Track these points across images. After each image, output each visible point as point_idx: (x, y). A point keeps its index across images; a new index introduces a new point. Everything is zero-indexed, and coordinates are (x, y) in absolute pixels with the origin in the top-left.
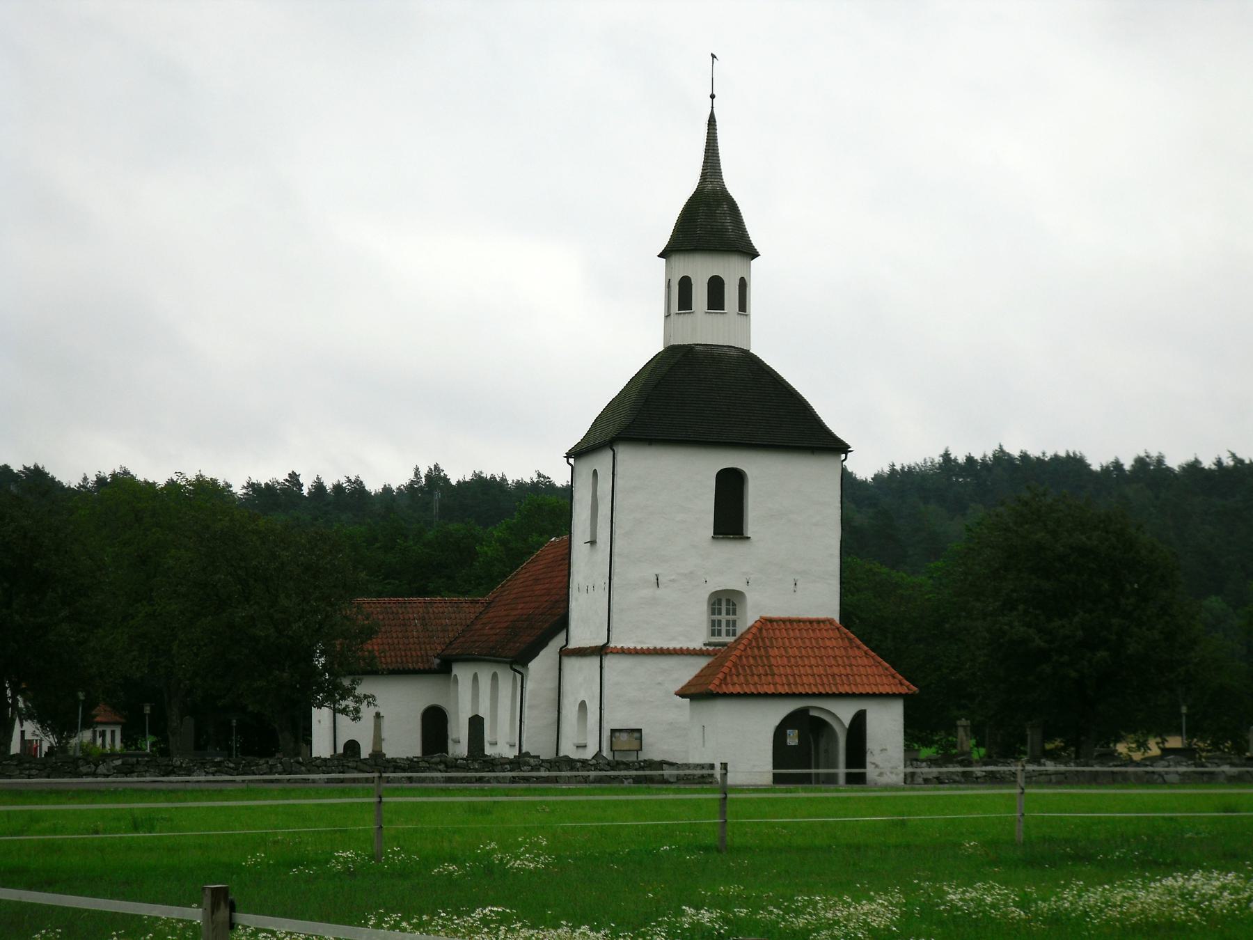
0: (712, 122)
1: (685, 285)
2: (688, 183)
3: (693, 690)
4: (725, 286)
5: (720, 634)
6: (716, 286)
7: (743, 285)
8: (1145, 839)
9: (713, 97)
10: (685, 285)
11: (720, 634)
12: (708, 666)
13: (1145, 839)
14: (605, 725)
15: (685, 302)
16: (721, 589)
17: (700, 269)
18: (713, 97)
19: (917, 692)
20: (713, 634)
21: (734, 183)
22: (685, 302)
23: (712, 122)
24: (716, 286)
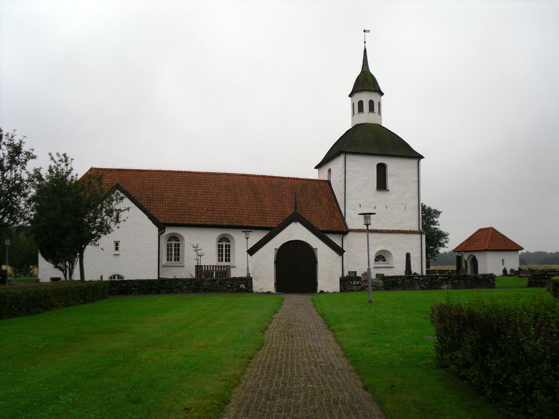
0: (365, 51)
1: (361, 103)
2: (358, 71)
3: (456, 250)
4: (374, 104)
5: (222, 261)
6: (371, 103)
7: (379, 104)
8: (93, 233)
9: (365, 42)
10: (361, 103)
11: (222, 261)
12: (340, 247)
13: (93, 233)
14: (345, 269)
15: (361, 109)
16: (297, 239)
17: (365, 97)
18: (365, 42)
19: (442, 250)
20: (219, 261)
21: (373, 70)
22: (361, 109)
23: (365, 51)
24: (371, 103)
